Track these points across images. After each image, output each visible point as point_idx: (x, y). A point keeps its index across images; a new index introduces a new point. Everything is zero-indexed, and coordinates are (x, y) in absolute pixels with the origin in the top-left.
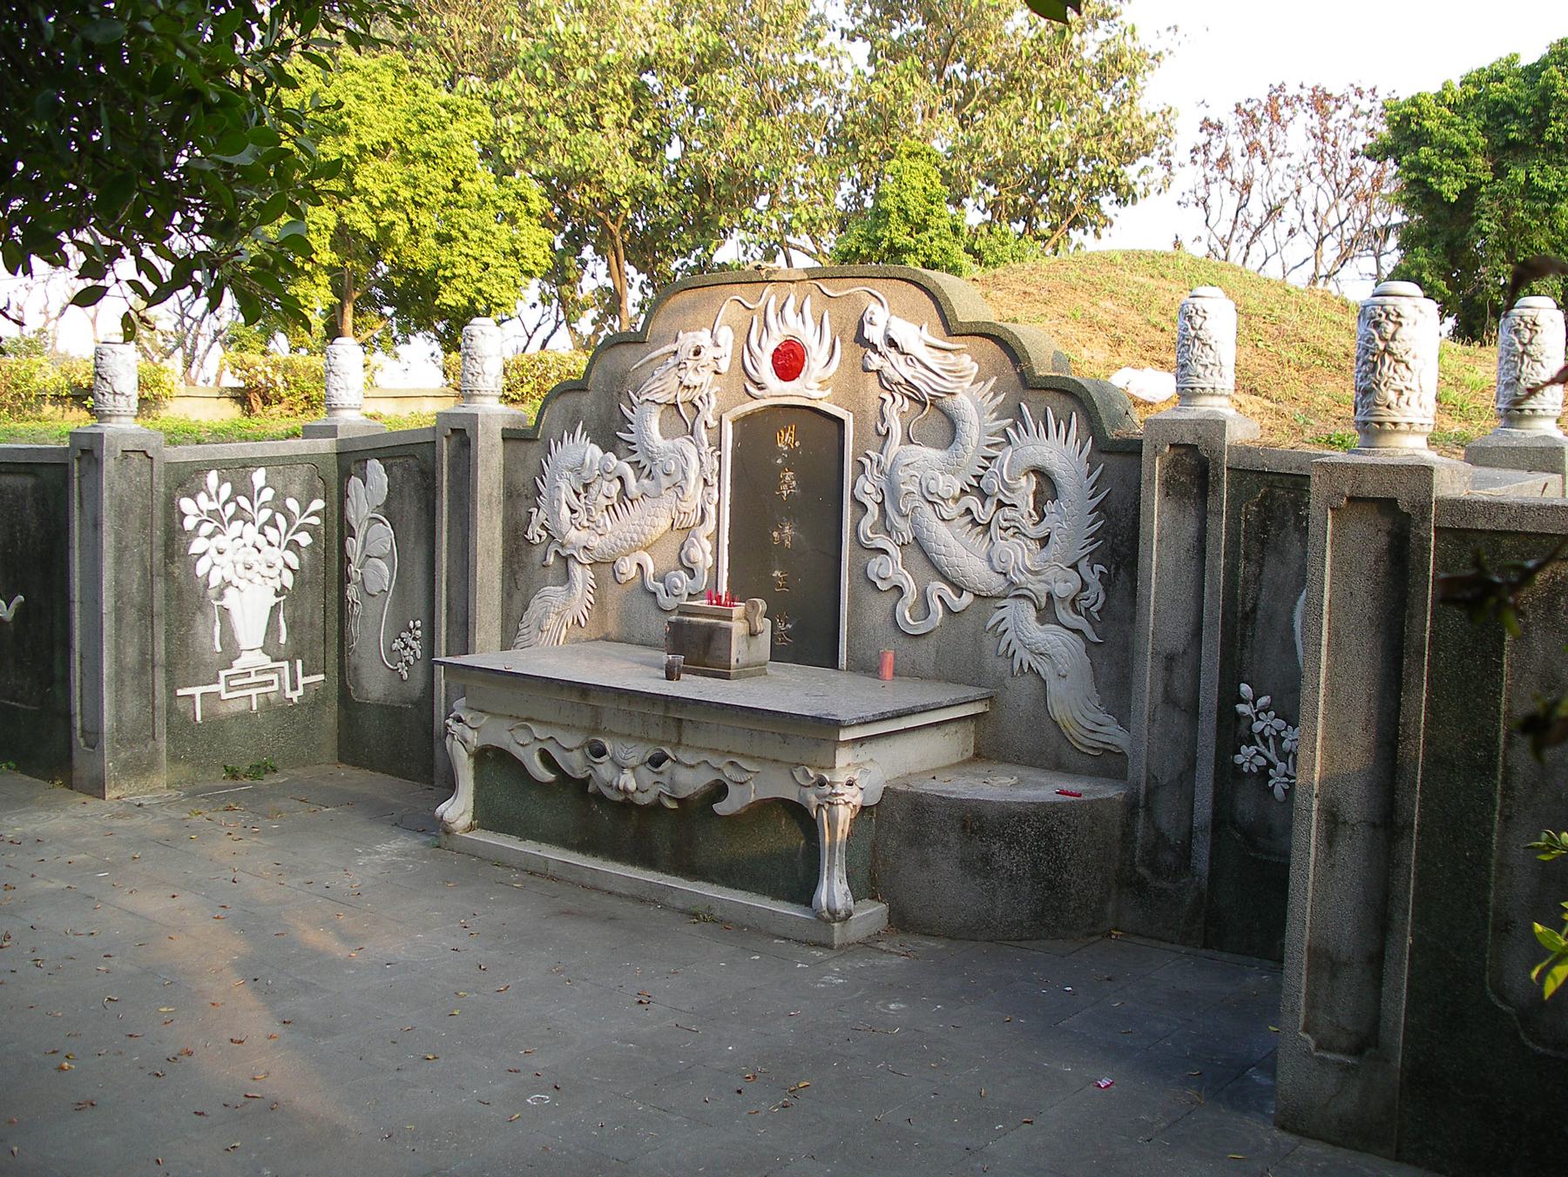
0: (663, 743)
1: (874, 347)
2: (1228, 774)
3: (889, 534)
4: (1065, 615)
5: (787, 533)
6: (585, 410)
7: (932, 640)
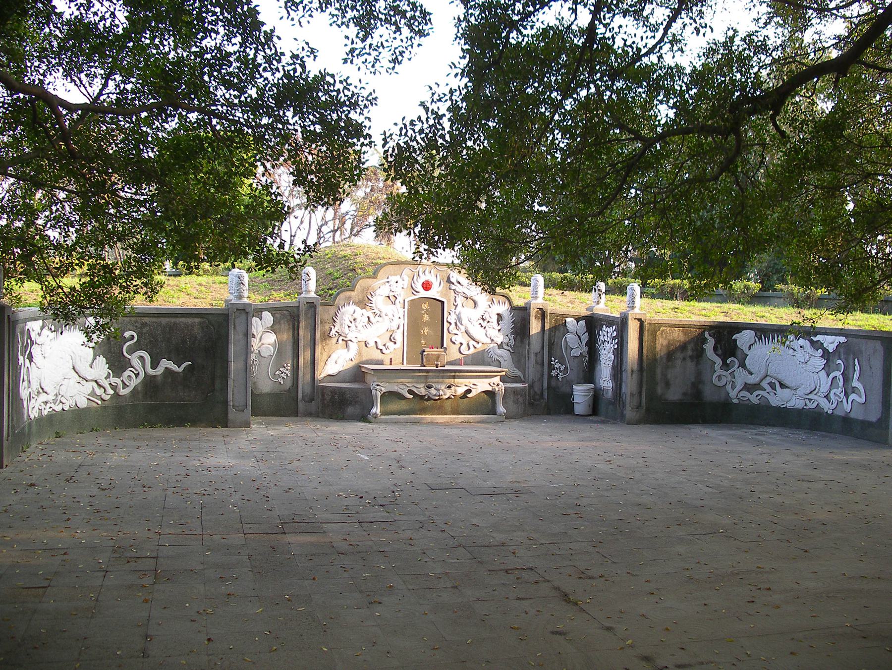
2: (550, 377)
4: (505, 347)
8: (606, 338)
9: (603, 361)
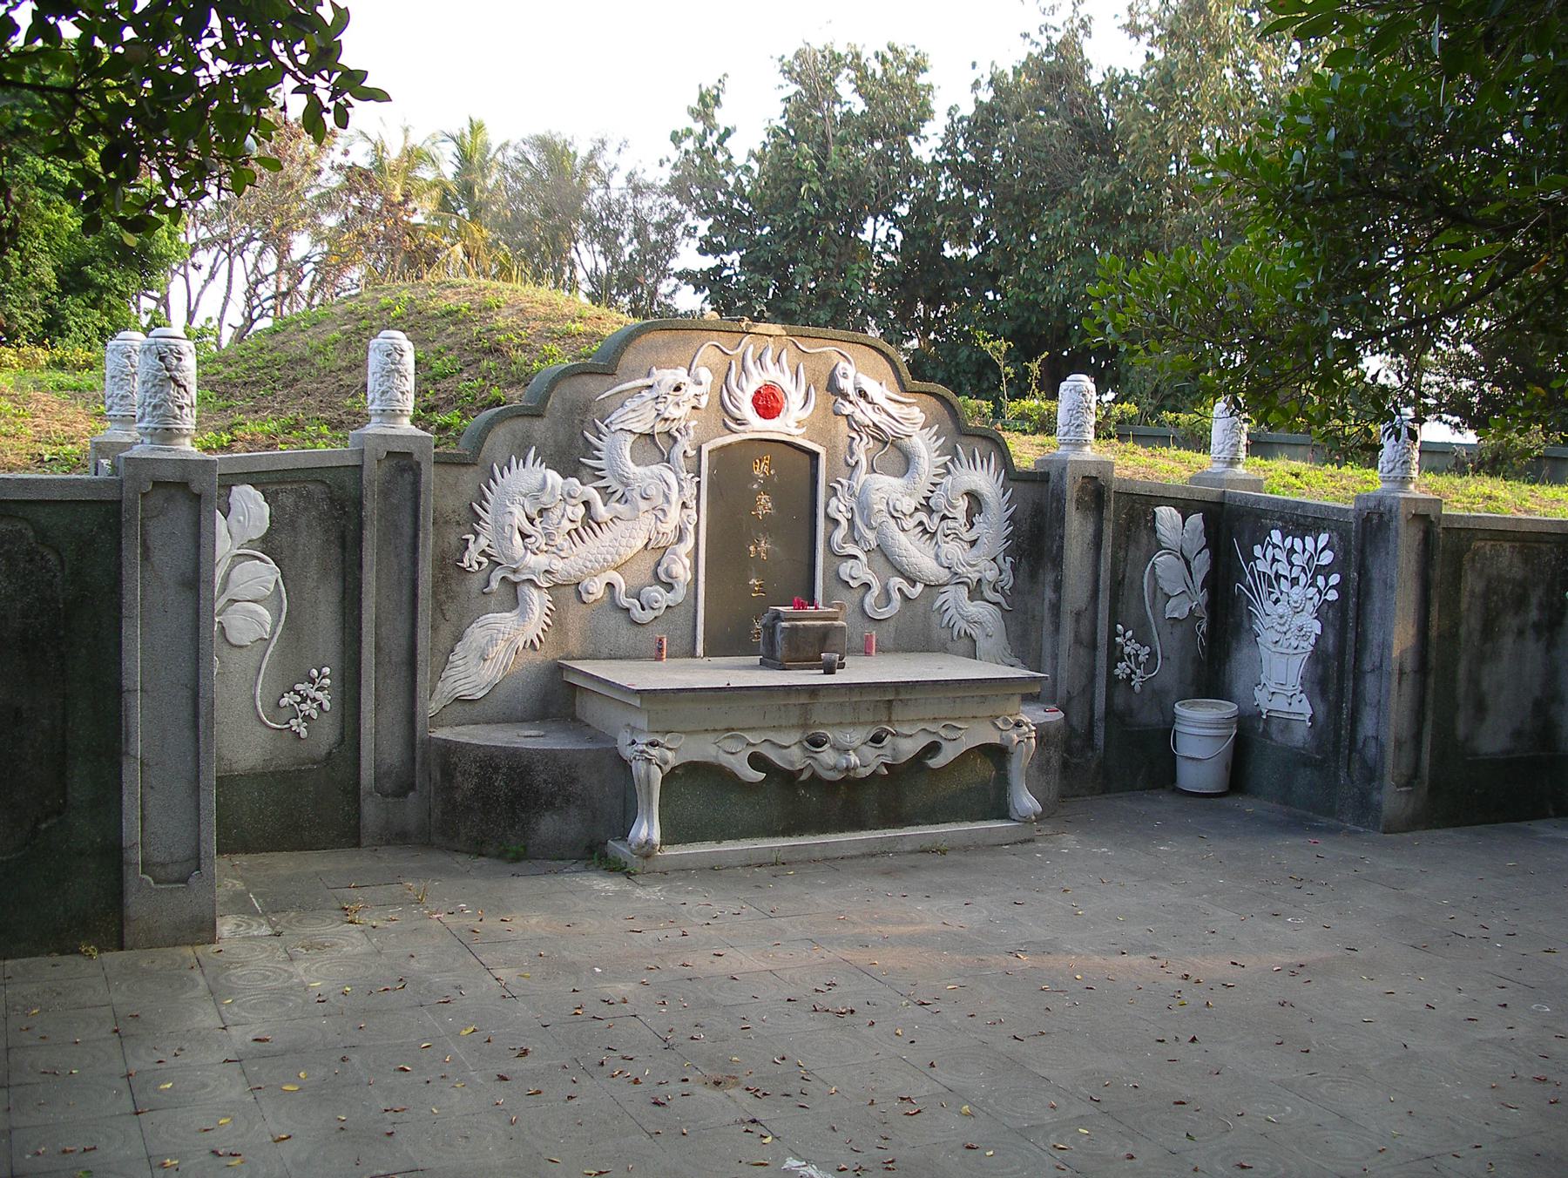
0: (880, 722)
1: (845, 396)
2: (1112, 680)
3: (856, 542)
5: (763, 547)
6: (537, 435)
7: (892, 623)
8: (1283, 568)
9: (1267, 638)
